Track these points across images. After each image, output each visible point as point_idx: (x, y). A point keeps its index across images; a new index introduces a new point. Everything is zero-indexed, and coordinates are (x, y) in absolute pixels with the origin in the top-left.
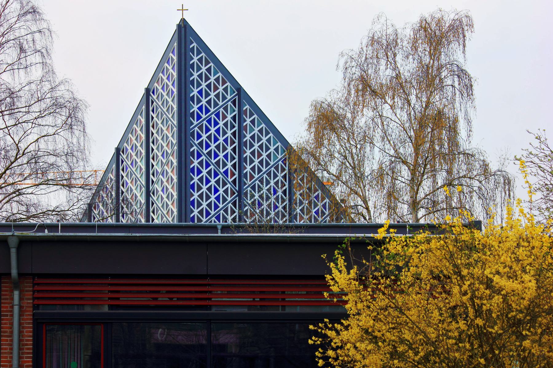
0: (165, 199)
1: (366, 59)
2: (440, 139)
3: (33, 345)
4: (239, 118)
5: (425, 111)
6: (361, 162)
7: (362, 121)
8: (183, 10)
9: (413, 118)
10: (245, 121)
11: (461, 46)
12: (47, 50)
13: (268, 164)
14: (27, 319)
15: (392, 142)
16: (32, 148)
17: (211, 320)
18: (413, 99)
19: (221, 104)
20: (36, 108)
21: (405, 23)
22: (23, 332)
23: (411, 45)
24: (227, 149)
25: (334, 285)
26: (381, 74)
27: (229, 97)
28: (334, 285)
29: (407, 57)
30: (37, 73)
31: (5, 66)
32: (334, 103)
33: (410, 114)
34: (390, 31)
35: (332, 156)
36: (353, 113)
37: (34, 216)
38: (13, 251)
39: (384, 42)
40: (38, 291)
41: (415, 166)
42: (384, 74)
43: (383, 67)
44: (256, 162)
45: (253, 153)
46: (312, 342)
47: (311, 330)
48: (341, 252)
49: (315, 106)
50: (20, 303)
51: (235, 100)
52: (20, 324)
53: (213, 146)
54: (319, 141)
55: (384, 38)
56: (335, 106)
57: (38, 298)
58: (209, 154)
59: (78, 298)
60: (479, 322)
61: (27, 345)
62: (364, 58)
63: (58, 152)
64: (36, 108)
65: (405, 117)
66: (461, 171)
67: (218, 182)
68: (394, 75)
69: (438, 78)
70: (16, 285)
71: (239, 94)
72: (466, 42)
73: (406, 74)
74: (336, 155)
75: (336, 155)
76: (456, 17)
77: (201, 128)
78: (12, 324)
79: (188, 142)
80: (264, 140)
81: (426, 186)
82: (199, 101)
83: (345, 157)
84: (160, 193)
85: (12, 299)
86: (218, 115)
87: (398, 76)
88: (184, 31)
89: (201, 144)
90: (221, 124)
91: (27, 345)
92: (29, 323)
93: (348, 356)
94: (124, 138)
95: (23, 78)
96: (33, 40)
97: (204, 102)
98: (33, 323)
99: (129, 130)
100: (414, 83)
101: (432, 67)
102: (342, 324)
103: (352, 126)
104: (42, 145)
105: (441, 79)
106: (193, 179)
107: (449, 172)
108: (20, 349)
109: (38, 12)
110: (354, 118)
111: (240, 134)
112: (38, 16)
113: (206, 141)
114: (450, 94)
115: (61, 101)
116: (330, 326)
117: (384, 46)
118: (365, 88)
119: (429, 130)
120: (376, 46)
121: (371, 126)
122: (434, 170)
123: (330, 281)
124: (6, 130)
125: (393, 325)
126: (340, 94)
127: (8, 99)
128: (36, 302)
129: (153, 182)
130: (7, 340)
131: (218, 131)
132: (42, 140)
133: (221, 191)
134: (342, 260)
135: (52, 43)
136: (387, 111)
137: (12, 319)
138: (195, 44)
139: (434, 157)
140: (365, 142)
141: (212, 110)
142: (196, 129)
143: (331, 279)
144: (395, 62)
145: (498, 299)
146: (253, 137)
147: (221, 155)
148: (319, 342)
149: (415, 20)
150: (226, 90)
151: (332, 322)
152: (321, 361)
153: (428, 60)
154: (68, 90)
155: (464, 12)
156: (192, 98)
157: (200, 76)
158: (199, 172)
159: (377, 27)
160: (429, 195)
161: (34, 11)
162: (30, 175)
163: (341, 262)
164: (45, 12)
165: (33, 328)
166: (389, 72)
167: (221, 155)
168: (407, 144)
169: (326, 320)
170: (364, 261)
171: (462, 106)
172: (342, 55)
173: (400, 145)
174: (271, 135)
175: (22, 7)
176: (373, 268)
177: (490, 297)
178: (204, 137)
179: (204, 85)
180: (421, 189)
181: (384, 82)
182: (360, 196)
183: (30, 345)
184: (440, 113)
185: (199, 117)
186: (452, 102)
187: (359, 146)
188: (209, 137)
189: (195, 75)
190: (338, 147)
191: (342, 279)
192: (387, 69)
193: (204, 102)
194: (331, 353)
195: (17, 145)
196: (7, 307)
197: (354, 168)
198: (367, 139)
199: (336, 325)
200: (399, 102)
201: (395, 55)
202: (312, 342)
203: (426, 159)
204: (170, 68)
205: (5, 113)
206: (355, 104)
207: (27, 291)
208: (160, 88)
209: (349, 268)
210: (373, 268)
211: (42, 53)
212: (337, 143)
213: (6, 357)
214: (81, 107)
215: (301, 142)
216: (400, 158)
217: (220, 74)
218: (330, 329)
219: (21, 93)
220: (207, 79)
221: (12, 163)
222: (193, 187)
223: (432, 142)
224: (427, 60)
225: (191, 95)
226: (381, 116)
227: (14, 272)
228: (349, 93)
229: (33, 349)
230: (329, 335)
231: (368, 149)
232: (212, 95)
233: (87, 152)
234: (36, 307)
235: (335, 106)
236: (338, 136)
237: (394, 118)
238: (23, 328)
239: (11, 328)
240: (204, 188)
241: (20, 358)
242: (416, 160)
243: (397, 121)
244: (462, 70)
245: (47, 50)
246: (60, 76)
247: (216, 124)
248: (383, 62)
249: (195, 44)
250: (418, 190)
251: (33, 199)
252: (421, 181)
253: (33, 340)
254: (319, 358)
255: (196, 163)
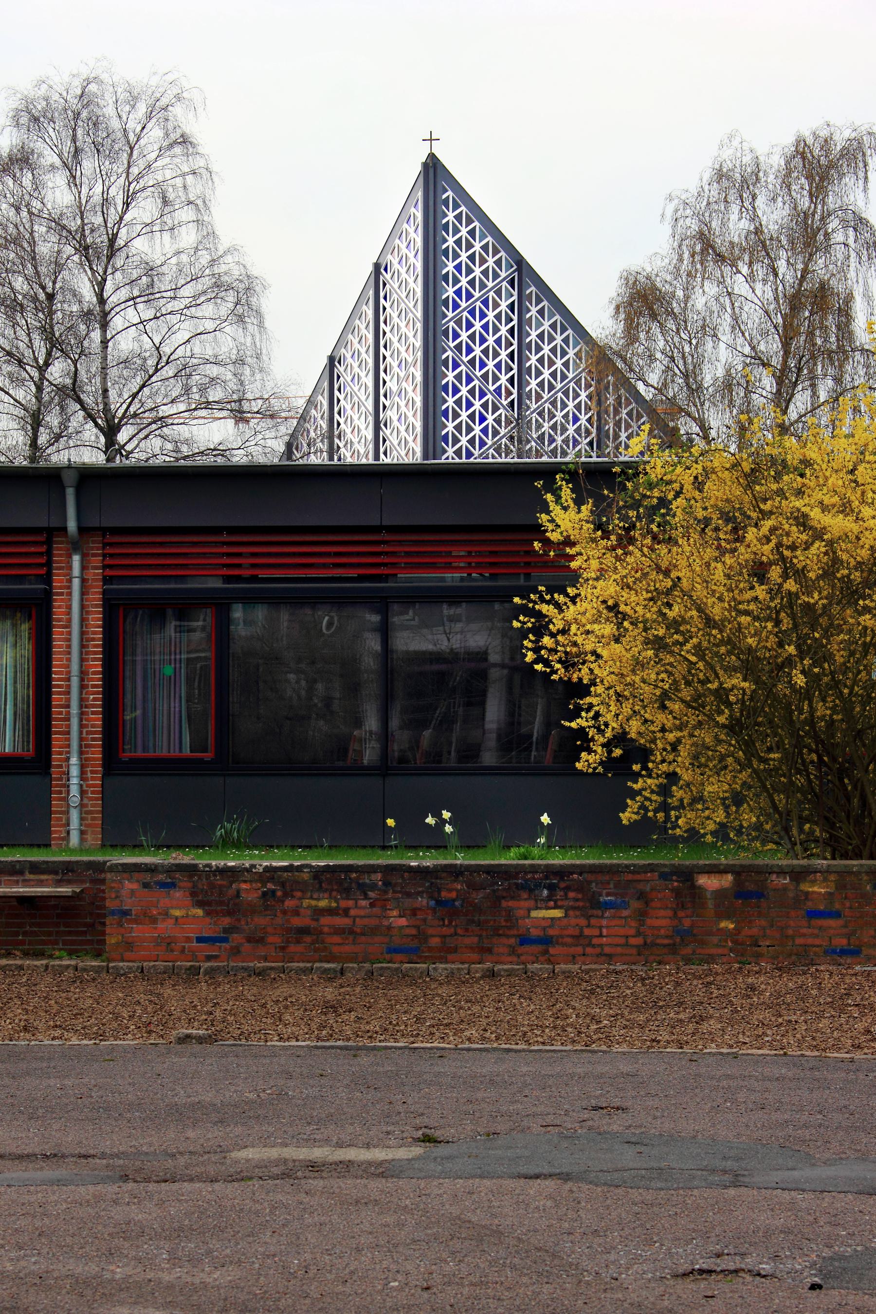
0: (403, 433)
1: (708, 204)
2: (824, 329)
3: (104, 639)
4: (519, 307)
5: (800, 285)
6: (698, 366)
7: (699, 301)
8: (431, 140)
9: (781, 295)
10: (529, 311)
11: (861, 182)
12: (204, 202)
13: (564, 377)
14: (94, 599)
15: (747, 334)
16: (180, 352)
17: (387, 597)
18: (781, 265)
19: (490, 284)
20: (187, 291)
21: (770, 143)
22: (88, 619)
23: (780, 181)
24: (499, 355)
25: (553, 531)
26: (731, 226)
27: (503, 274)
28: (553, 531)
29: (774, 200)
30: (188, 237)
31: (139, 227)
32: (657, 275)
33: (776, 289)
34: (747, 159)
35: (652, 358)
36: (685, 289)
37: (185, 458)
38: (70, 494)
39: (738, 176)
40: (112, 556)
41: (782, 371)
42: (736, 227)
43: (734, 217)
44: (546, 374)
45: (541, 361)
46: (519, 625)
47: (517, 604)
48: (567, 477)
49: (627, 279)
50: (82, 574)
51: (513, 279)
52: (82, 607)
53: (478, 351)
54: (631, 334)
55: (738, 170)
56: (658, 279)
57: (111, 567)
58: (472, 362)
59: (176, 566)
60: (791, 585)
61: (93, 640)
62: (705, 203)
63: (220, 358)
64: (187, 291)
65: (770, 295)
66: (856, 377)
67: (485, 406)
68: (752, 228)
69: (822, 232)
70: (76, 547)
71: (519, 270)
72: (869, 173)
73: (771, 227)
74: (659, 355)
75: (659, 355)
76: (854, 135)
77: (459, 323)
78: (69, 607)
79: (438, 346)
80: (559, 339)
81: (801, 401)
82: (456, 281)
83: (672, 359)
84: (396, 423)
85: (70, 568)
86: (485, 302)
87: (758, 231)
88: (433, 172)
89: (458, 347)
90: (491, 315)
91: (93, 640)
92: (96, 606)
93: (575, 644)
94: (341, 341)
95: (167, 245)
96: (185, 187)
97: (464, 281)
98: (103, 606)
99: (348, 327)
100: (784, 242)
101: (813, 215)
102: (567, 595)
103: (685, 309)
104: (197, 347)
105: (827, 235)
106: (446, 401)
107: (838, 380)
108: (82, 646)
109: (191, 143)
110: (687, 298)
111: (519, 332)
112: (191, 150)
113: (467, 343)
114: (840, 256)
115: (225, 278)
116: (548, 597)
117: (737, 183)
118: (706, 250)
119: (807, 314)
120: (725, 183)
121: (714, 308)
122: (813, 378)
123: (548, 524)
124: (141, 326)
125: (650, 595)
126: (667, 261)
127: (144, 278)
128: (109, 572)
129: (385, 407)
130: (62, 633)
131: (485, 327)
132: (196, 341)
133: (490, 419)
134: (569, 490)
135: (213, 190)
136: (740, 286)
137: (70, 600)
138: (450, 193)
139: (813, 357)
140: (705, 334)
141: (477, 294)
142: (452, 324)
143: (549, 521)
144: (754, 207)
145: (818, 547)
146: (541, 336)
147: (491, 365)
148: (530, 625)
149: (788, 141)
150: (498, 263)
151: (551, 590)
152: (530, 654)
153: (807, 204)
154: (238, 263)
155: (867, 126)
156: (446, 277)
157: (458, 242)
158: (456, 390)
159: (727, 154)
160: (805, 415)
161: (184, 141)
162: (49, 354)
163: (567, 493)
164: (201, 142)
165: (104, 613)
166: (745, 225)
167: (491, 365)
168: (770, 337)
169: (541, 588)
170: (606, 492)
171: (860, 275)
172: (670, 198)
173: (759, 338)
174: (570, 332)
175: (167, 135)
176: (621, 503)
177: (807, 546)
178: (464, 336)
179: (464, 256)
180: (792, 407)
181: (736, 240)
182: (694, 419)
183: (98, 640)
184: (824, 288)
185: (456, 306)
186: (843, 270)
187: (694, 342)
188: (472, 337)
189: (451, 241)
190: (661, 343)
191: (567, 521)
192: (740, 219)
193: (464, 281)
194: (547, 641)
195: (158, 349)
196: (61, 581)
197: (686, 376)
198: (708, 330)
199: (556, 596)
200: (760, 271)
201: (754, 197)
202: (519, 625)
203: (801, 359)
204: (411, 230)
205: (138, 300)
206: (689, 274)
207: (94, 555)
208: (395, 262)
209: (579, 502)
210: (621, 503)
211: (197, 205)
212: (660, 337)
213: (61, 660)
214: (257, 288)
215: (603, 336)
216: (760, 359)
217: (489, 239)
218: (548, 603)
219: (165, 269)
220: (469, 246)
221: (151, 377)
222: (445, 413)
223: (811, 334)
224: (805, 203)
225: (444, 272)
226: (729, 294)
227: (72, 525)
228: (681, 260)
229: (104, 646)
230: (544, 611)
231: (709, 345)
232: (477, 271)
233: (265, 358)
234: (107, 580)
235: (658, 279)
236: (662, 326)
237: (750, 296)
238: (88, 613)
239: (69, 613)
240: (464, 415)
241: (82, 660)
242: (785, 361)
243: (756, 301)
244: (861, 219)
245: (204, 202)
246: (224, 243)
247: (483, 315)
248: (735, 208)
249: (450, 193)
250: (787, 407)
251: (183, 431)
252: (793, 395)
253: (104, 633)
254: (528, 649)
255: (451, 376)
